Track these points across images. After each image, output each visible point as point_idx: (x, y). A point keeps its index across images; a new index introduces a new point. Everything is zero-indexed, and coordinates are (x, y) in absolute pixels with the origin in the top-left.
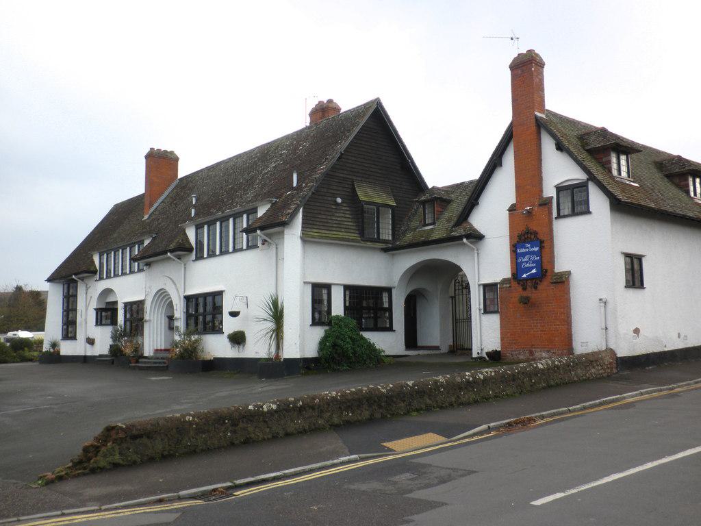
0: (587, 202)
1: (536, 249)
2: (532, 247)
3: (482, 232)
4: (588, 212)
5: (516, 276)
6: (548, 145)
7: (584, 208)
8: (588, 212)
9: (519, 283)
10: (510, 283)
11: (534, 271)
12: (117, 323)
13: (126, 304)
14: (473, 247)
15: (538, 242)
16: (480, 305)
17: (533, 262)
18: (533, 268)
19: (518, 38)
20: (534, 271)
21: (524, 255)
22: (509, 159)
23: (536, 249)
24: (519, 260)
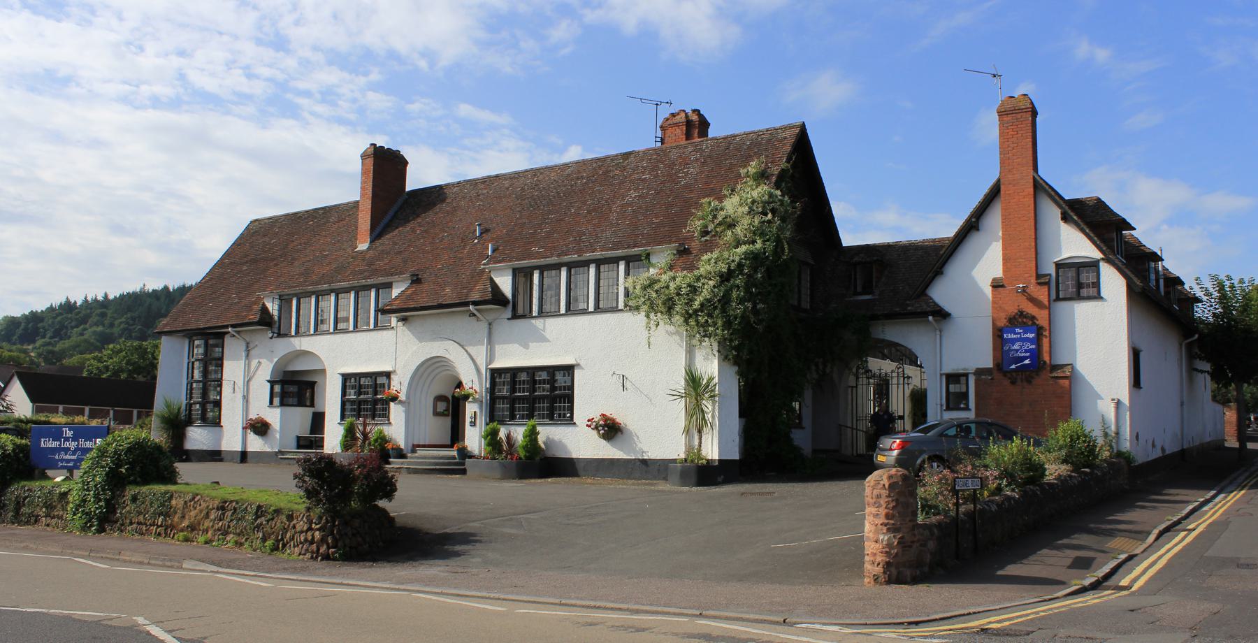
0: (1097, 285)
1: (1031, 336)
2: (1025, 333)
3: (950, 312)
4: (1098, 297)
5: (999, 366)
6: (1052, 213)
7: (1092, 291)
8: (1098, 297)
9: (1005, 376)
10: (991, 375)
11: (1027, 362)
12: (151, 406)
13: (346, 378)
14: (936, 326)
15: (1035, 327)
16: (941, 399)
17: (1026, 351)
18: (1026, 358)
19: (1000, 76)
20: (1027, 362)
21: (1014, 341)
22: (994, 220)
23: (1031, 336)
24: (1006, 348)
